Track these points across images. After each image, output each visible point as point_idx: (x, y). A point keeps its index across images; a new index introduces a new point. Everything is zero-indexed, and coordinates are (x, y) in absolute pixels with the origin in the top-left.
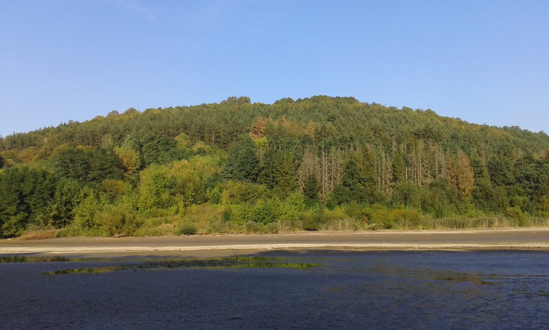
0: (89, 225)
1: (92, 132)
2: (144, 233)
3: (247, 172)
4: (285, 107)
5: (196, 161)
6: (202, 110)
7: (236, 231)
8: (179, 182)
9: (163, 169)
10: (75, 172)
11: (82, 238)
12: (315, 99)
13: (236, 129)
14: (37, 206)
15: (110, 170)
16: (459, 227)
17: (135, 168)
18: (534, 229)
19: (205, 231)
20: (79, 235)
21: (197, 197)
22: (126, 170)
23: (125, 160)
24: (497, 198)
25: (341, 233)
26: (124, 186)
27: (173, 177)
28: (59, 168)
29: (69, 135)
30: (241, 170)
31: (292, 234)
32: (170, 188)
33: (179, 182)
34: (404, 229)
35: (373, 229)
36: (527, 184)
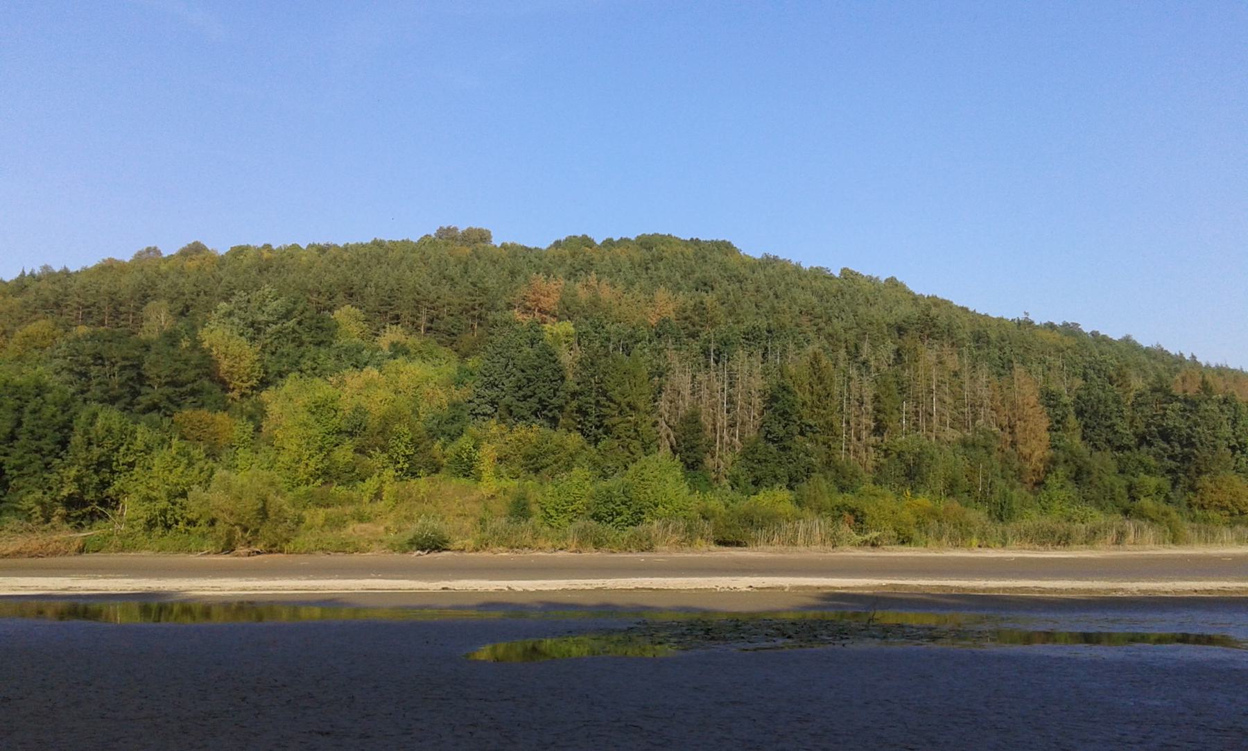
0: (161, 523)
1: (112, 296)
2: (312, 546)
3: (541, 401)
4: (577, 256)
5: (398, 372)
6: (379, 252)
7: (550, 543)
8: (373, 423)
9: (322, 389)
10: (105, 387)
11: (146, 556)
12: (646, 243)
13: (480, 300)
14: (25, 471)
15: (195, 386)
16: (1059, 543)
17: (248, 385)
18: (1198, 550)
19: (470, 542)
20: (134, 548)
21: (418, 458)
22: (225, 387)
23: (225, 365)
24: (1100, 479)
25: (800, 553)
26: (231, 426)
27: (357, 409)
28: (65, 376)
29: (52, 299)
30: (525, 398)
31: (687, 554)
32: (351, 434)
33: (373, 423)
34: (940, 546)
35: (873, 545)
36: (1164, 450)
